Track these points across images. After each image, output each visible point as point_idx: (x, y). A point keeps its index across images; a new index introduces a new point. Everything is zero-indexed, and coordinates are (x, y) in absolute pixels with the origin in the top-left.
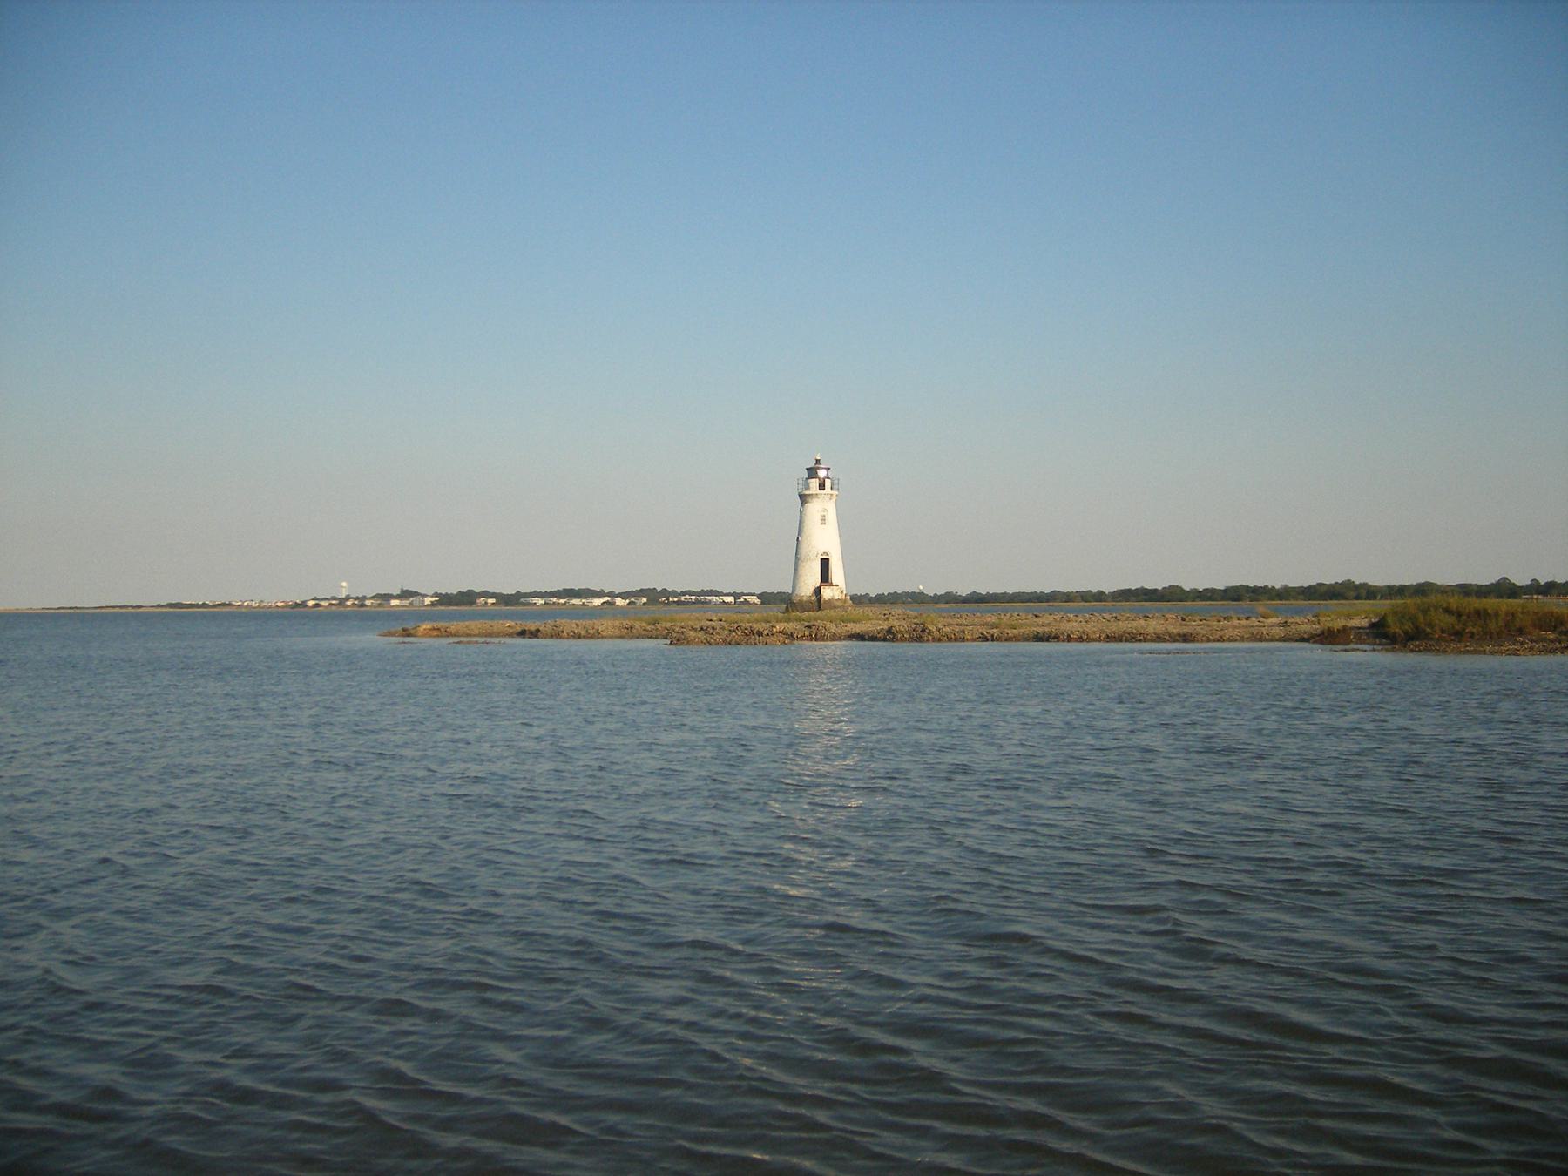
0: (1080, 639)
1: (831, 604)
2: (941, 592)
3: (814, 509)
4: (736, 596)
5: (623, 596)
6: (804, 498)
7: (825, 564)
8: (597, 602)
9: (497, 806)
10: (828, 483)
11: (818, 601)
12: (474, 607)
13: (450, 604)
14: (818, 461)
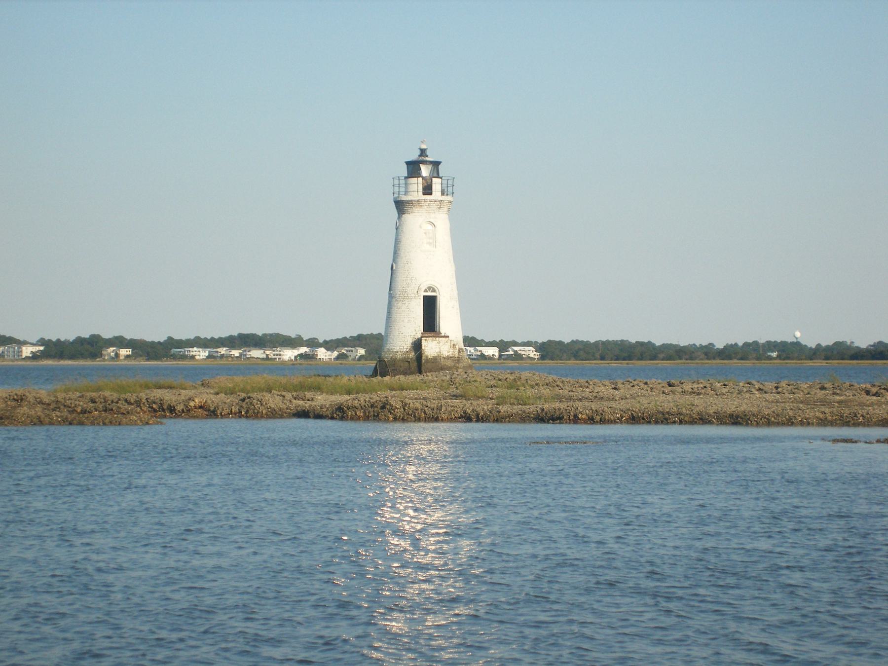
0: (591, 420)
1: (437, 365)
2: (827, 341)
3: (415, 220)
4: (503, 346)
5: (329, 345)
6: (401, 206)
7: (430, 305)
8: (289, 354)
9: (809, 529)
10: (437, 184)
11: (417, 362)
12: (97, 362)
13: (61, 356)
14: (423, 152)
